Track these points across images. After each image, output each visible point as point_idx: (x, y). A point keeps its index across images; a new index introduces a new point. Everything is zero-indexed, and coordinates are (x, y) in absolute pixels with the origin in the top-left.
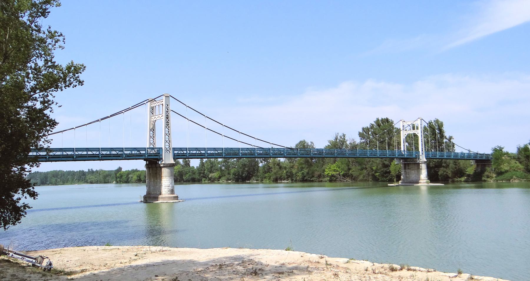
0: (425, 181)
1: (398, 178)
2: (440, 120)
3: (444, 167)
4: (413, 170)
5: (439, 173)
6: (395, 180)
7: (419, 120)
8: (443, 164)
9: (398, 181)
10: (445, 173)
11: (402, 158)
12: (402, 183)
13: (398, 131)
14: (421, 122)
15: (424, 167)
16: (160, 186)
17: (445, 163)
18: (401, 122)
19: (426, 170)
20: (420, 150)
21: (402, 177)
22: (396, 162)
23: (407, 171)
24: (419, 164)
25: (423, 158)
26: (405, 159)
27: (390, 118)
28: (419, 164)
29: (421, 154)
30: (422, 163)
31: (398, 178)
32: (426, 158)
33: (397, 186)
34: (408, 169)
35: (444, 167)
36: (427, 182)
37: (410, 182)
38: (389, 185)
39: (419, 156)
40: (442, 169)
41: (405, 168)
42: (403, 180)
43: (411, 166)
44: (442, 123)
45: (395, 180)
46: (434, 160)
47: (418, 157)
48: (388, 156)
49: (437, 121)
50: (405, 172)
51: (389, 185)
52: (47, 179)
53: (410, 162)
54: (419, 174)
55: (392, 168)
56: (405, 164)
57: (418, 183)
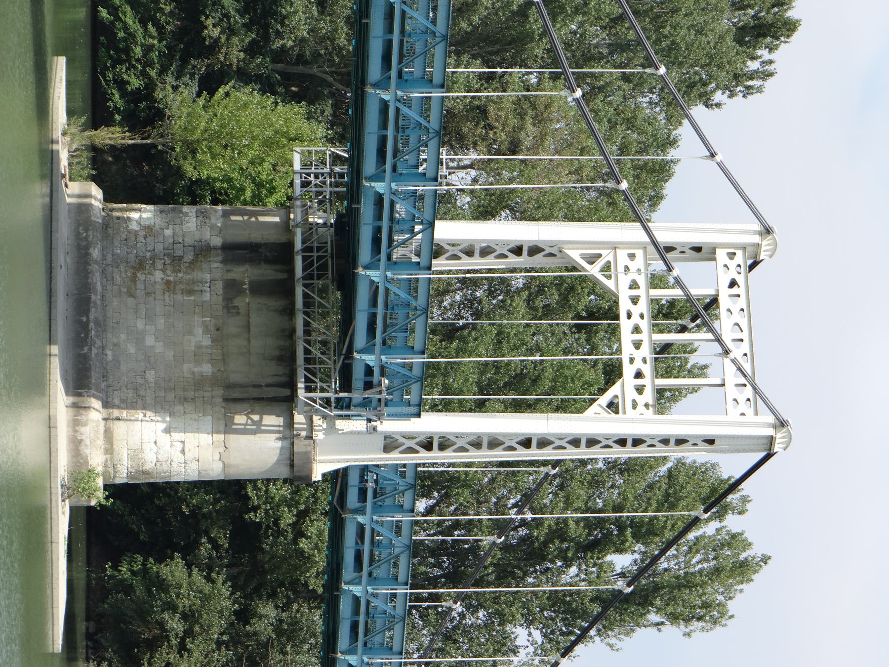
0: (96, 460)
1: (138, 172)
2: (745, 601)
3: (244, 615)
4: (219, 335)
5: (174, 570)
6: (112, 136)
7: (760, 425)
8: (268, 610)
9: (103, 167)
10: (176, 625)
11: (346, 227)
12: (82, 210)
13: (633, 185)
14: (738, 444)
15: (251, 449)
16: (142, 203)
17: (288, 633)
18: (746, 232)
19: (215, 471)
20: (432, 423)
21: (142, 214)
22: (305, 148)
23: (213, 273)
24: (285, 402)
25: (339, 444)
26: (337, 261)
27: (785, 56)
28: (285, 402)
29: (388, 426)
30: (289, 431)
31: (138, 172)
32: (338, 478)
33: (49, 158)
34: (232, 288)
35: (244, 615)
36: (80, 476)
37: (82, 302)
38: (60, 68)
39: (374, 408)
40: (224, 598)
41: (237, 251)
42: (109, 225)
43: (260, 314)
44: (709, 613)
45: (112, 136)
46: (318, 526)
47: (351, 390)
48: (375, 96)
49: (735, 565)
50: (203, 251)
51: (60, 68)
52: (279, 426)
53: (305, 307)
54: (174, 397)
55: (248, 110)
56: (281, 253)
57: (80, 382)
